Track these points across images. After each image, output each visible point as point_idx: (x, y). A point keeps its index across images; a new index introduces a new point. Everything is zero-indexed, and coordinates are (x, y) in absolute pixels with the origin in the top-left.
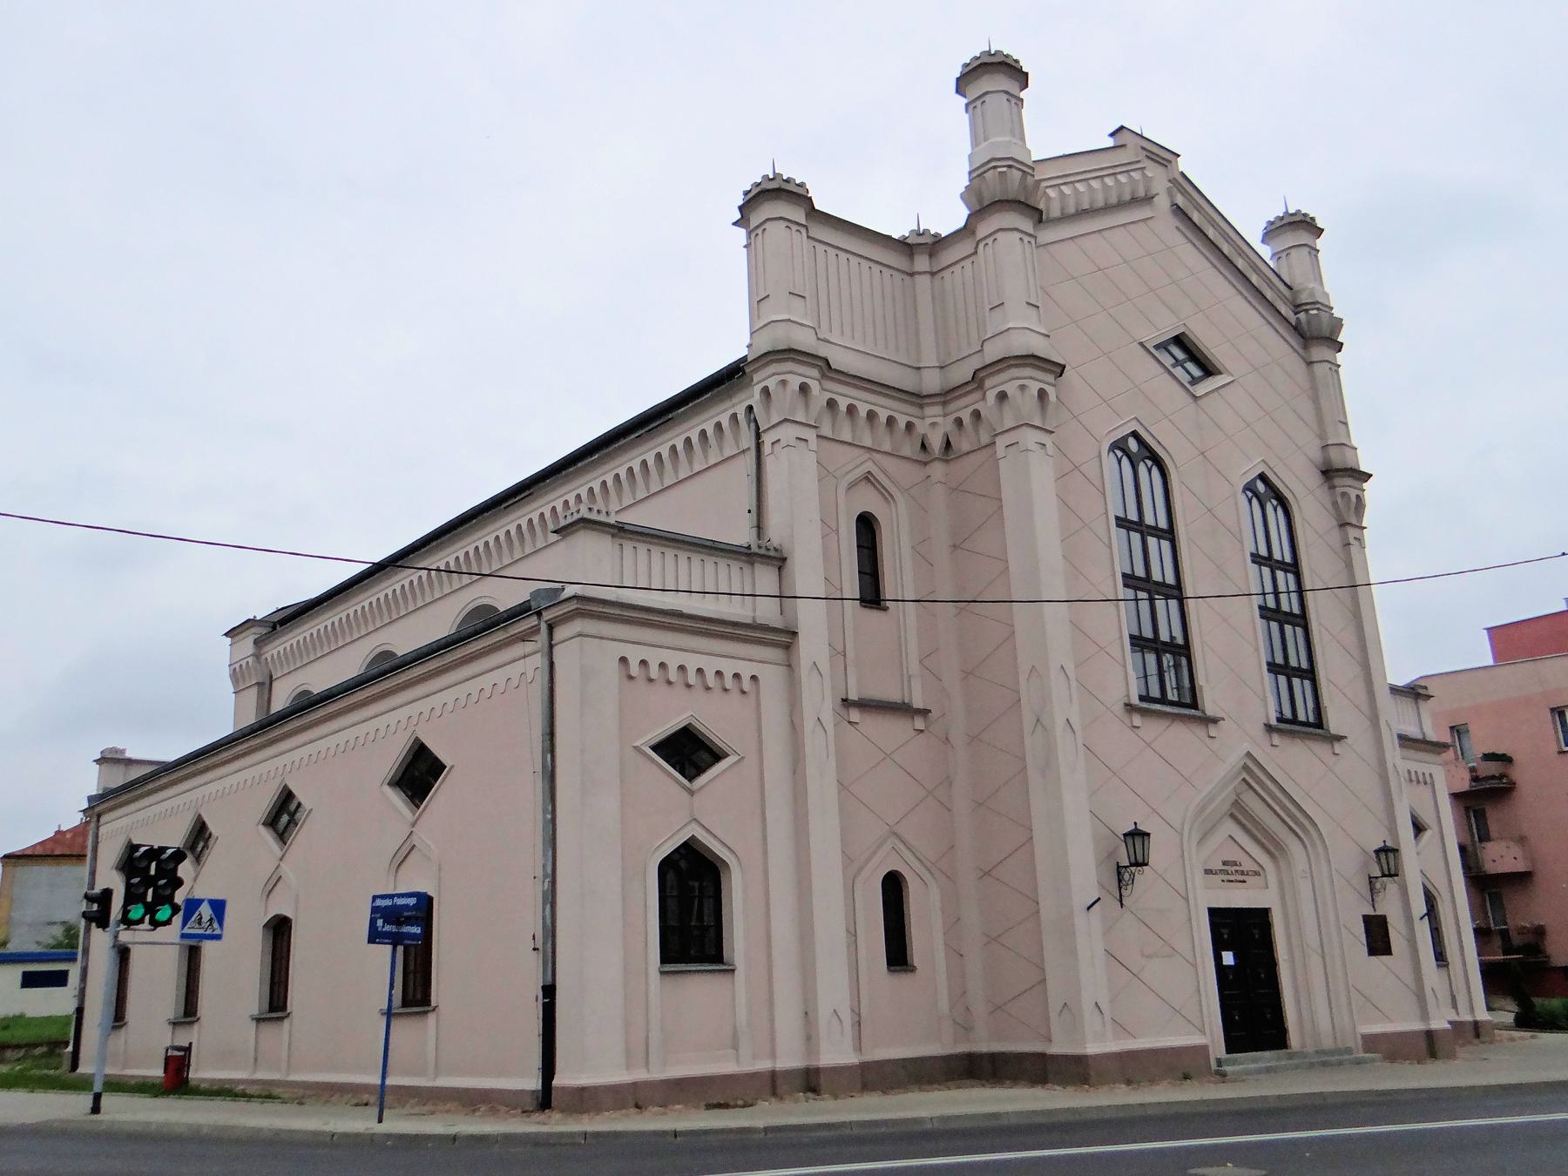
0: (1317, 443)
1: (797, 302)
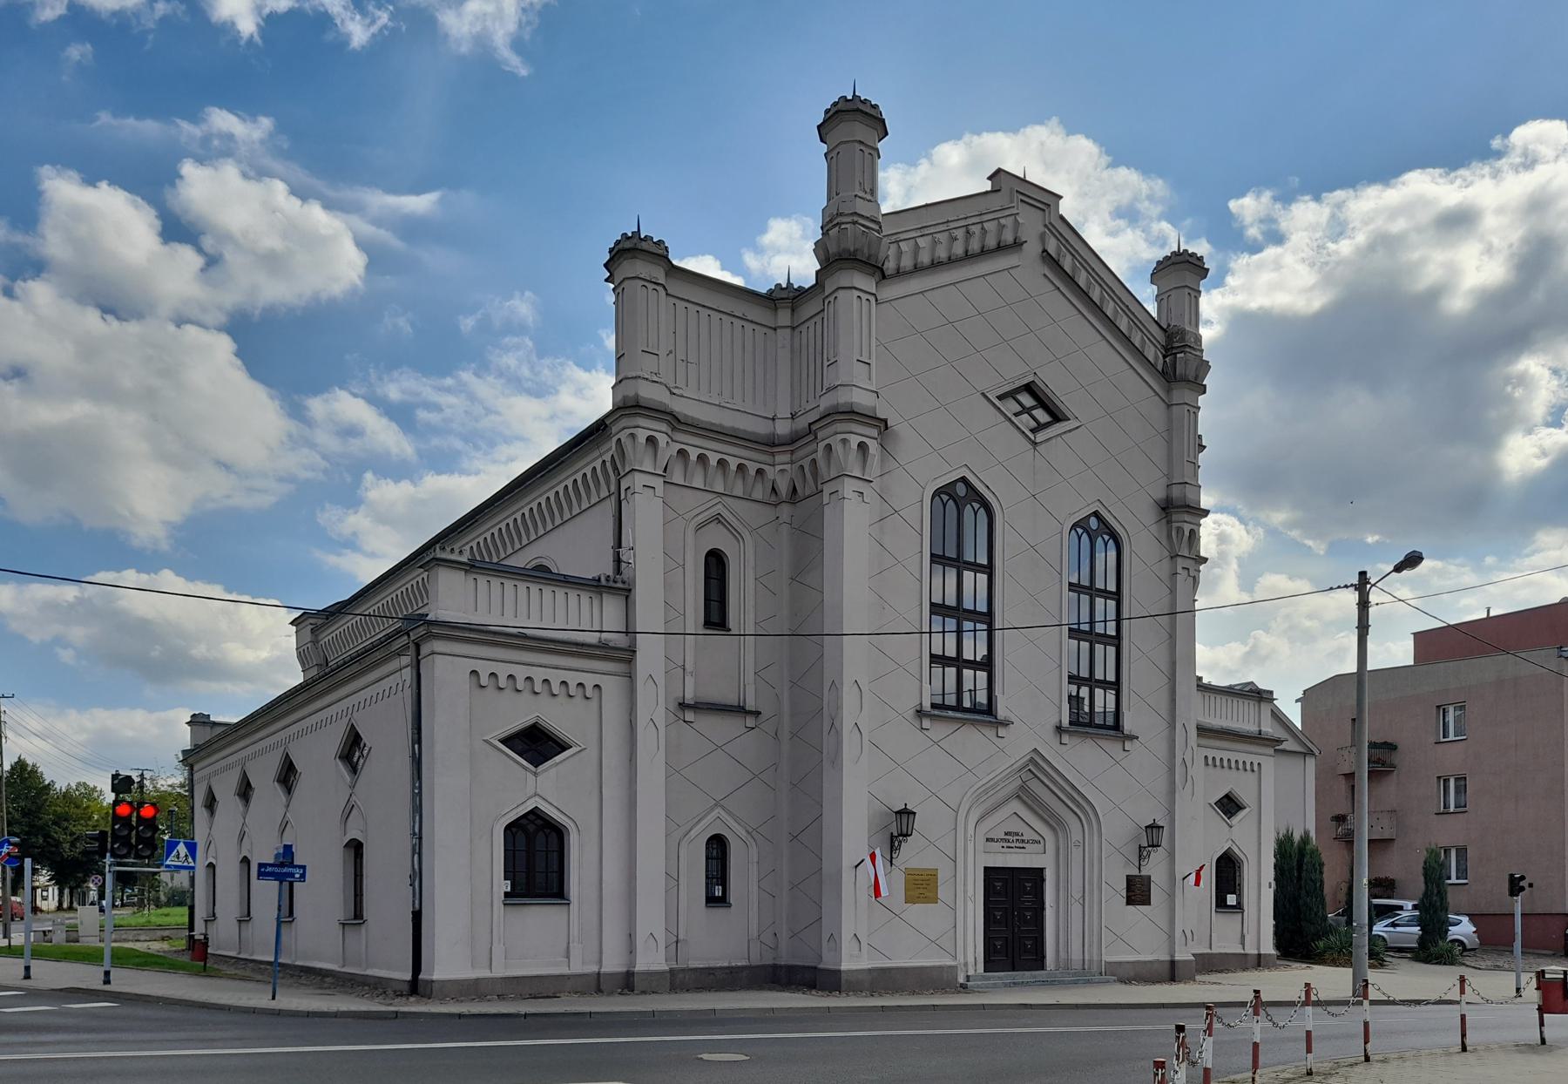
0: (1164, 481)
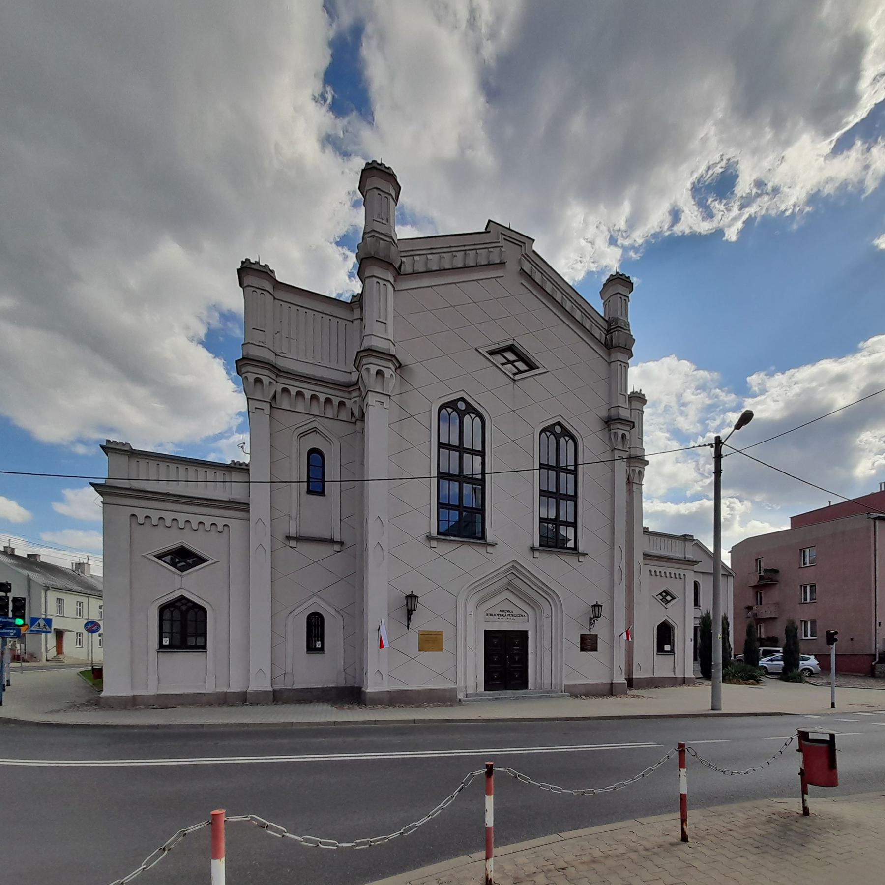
0: (607, 407)
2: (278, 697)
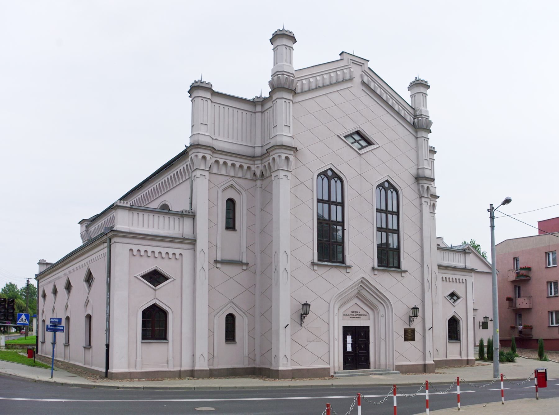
0: (416, 167)
1: (203, 127)
2: (213, 374)
